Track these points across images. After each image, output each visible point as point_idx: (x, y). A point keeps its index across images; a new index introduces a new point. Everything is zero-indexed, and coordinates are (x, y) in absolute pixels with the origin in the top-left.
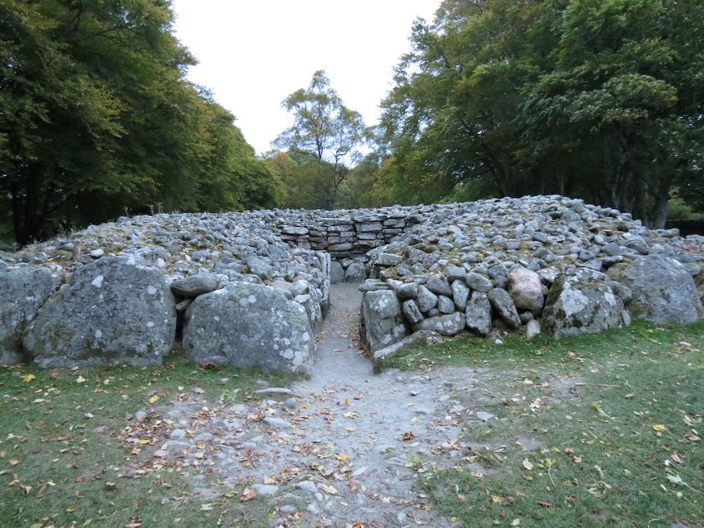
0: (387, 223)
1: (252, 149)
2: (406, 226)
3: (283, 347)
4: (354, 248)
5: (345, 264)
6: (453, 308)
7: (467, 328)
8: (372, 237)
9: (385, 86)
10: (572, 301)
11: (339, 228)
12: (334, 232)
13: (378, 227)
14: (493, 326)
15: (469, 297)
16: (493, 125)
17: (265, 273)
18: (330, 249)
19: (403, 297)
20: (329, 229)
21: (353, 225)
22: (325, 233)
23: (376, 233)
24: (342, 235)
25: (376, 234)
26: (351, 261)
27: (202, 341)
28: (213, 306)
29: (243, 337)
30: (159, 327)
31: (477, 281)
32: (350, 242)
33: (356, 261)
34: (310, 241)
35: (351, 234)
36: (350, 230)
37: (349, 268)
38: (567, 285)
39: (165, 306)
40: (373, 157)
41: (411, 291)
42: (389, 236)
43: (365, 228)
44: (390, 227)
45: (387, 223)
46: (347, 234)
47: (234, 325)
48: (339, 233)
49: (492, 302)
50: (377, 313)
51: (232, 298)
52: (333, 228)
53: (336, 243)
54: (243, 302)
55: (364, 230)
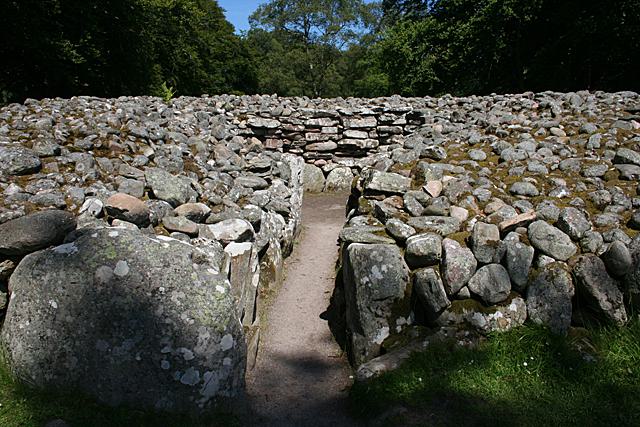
1: (230, 27)
4: (339, 148)
5: (326, 169)
8: (363, 135)
11: (321, 122)
13: (371, 122)
17: (178, 196)
19: (416, 261)
20: (308, 123)
22: (302, 128)
24: (324, 130)
25: (368, 132)
32: (334, 140)
33: (341, 166)
40: (366, 40)
45: (383, 118)
46: (330, 130)
48: (320, 128)
52: (313, 122)
53: (316, 141)
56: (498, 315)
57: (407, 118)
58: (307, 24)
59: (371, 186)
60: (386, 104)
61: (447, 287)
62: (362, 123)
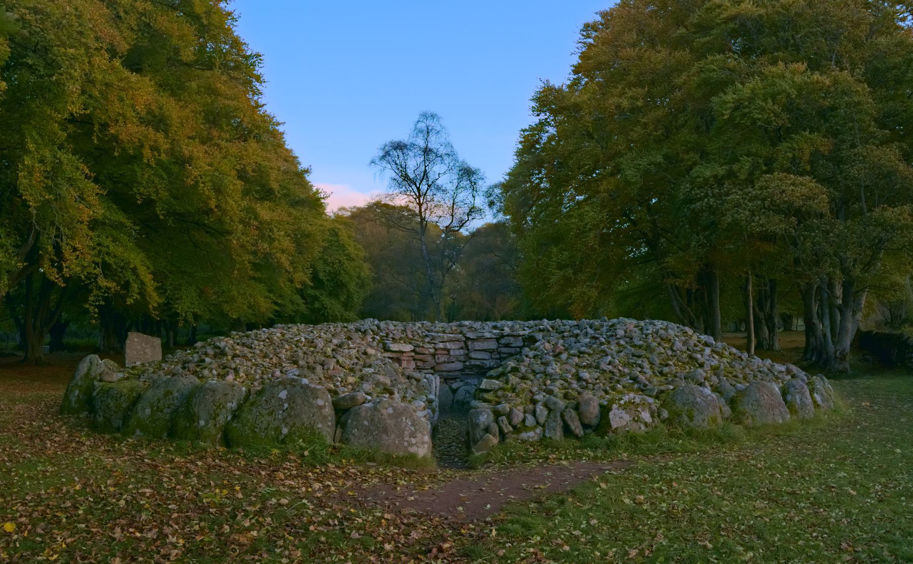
0: (503, 341)
1: (299, 163)
4: (465, 367)
6: (535, 423)
10: (619, 418)
13: (493, 345)
16: (647, 201)
18: (436, 368)
20: (437, 346)
22: (432, 351)
23: (491, 351)
24: (452, 353)
33: (467, 384)
34: (414, 360)
36: (462, 348)
37: (459, 392)
38: (615, 406)
42: (505, 355)
43: (478, 345)
44: (507, 345)
46: (457, 352)
48: (448, 350)
52: (441, 345)
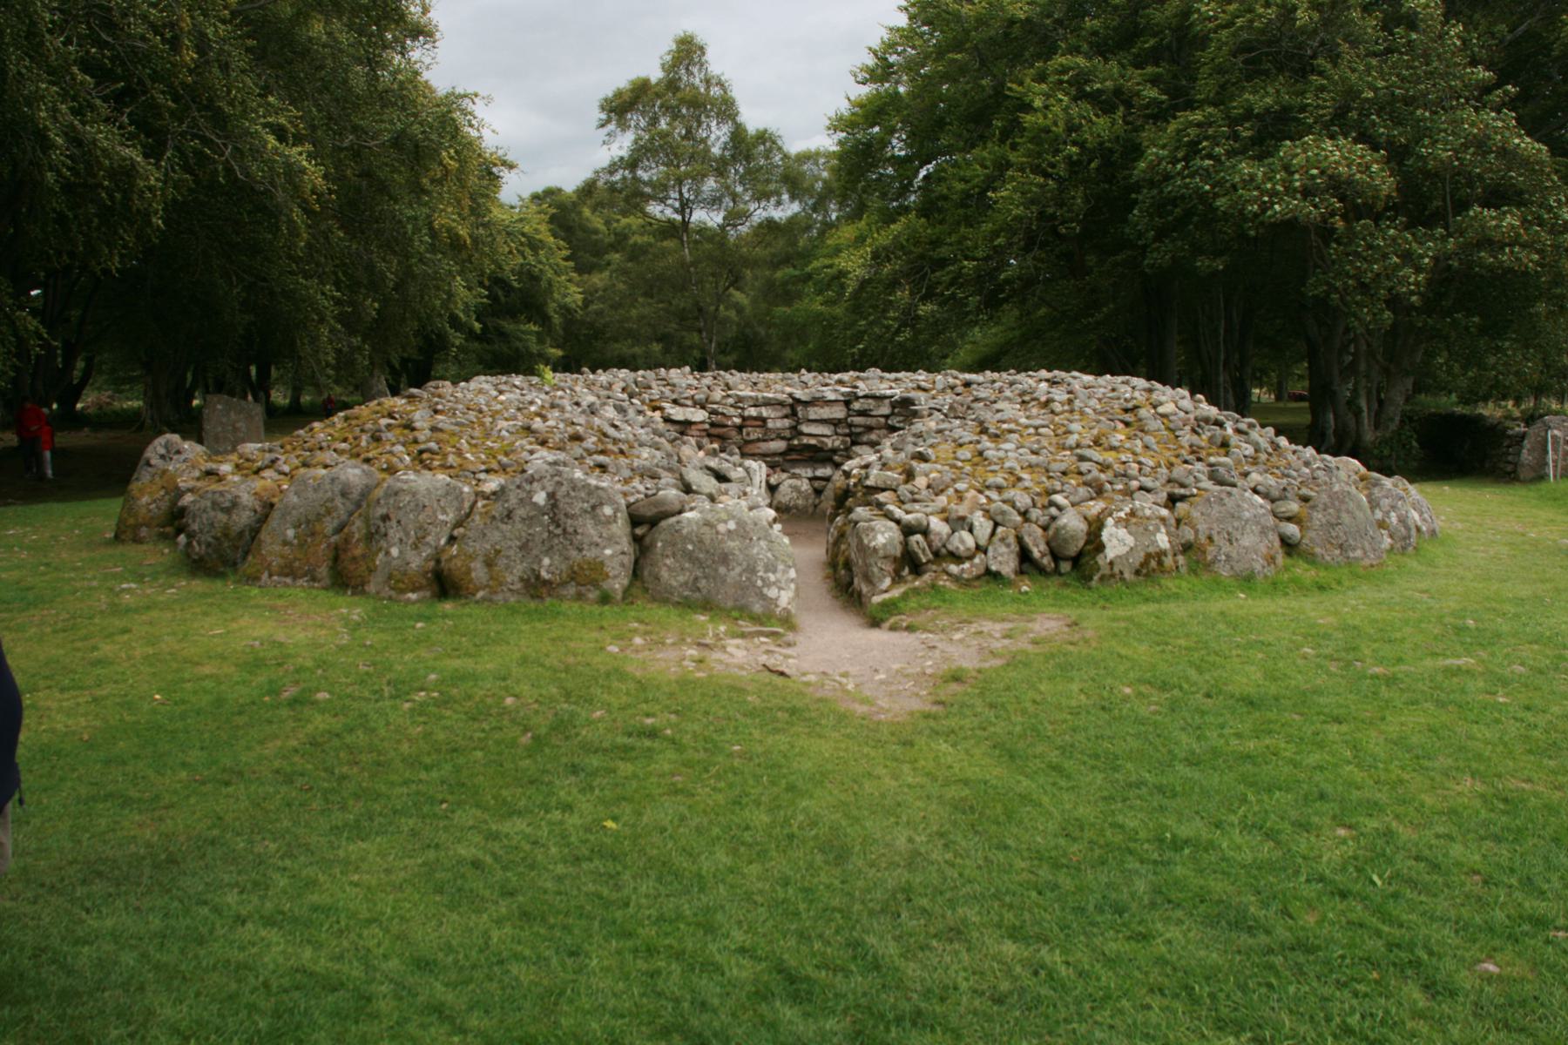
0: (856, 406)
2: (893, 414)
3: (767, 584)
7: (988, 572)
9: (841, 90)
11: (765, 412)
12: (755, 419)
13: (838, 412)
14: (1020, 572)
15: (993, 534)
16: (1050, 212)
19: (908, 530)
20: (746, 413)
21: (792, 406)
22: (737, 421)
23: (835, 423)
24: (770, 424)
25: (835, 425)
26: (785, 475)
27: (670, 571)
28: (685, 532)
29: (722, 570)
30: (614, 551)
31: (1003, 513)
32: (783, 438)
33: (794, 476)
35: (787, 423)
36: (786, 417)
37: (782, 488)
38: (1110, 521)
39: (621, 528)
41: (920, 524)
42: (859, 430)
43: (813, 413)
45: (856, 406)
46: (779, 424)
47: (710, 556)
48: (764, 420)
49: (1020, 540)
50: (875, 550)
51: (707, 524)
52: (753, 412)
53: (759, 440)
54: (721, 528)
55: (812, 417)
56: (967, 565)
57: (893, 405)
58: (685, 206)
59: (868, 483)
60: (860, 384)
61: (930, 546)
62: (825, 413)
